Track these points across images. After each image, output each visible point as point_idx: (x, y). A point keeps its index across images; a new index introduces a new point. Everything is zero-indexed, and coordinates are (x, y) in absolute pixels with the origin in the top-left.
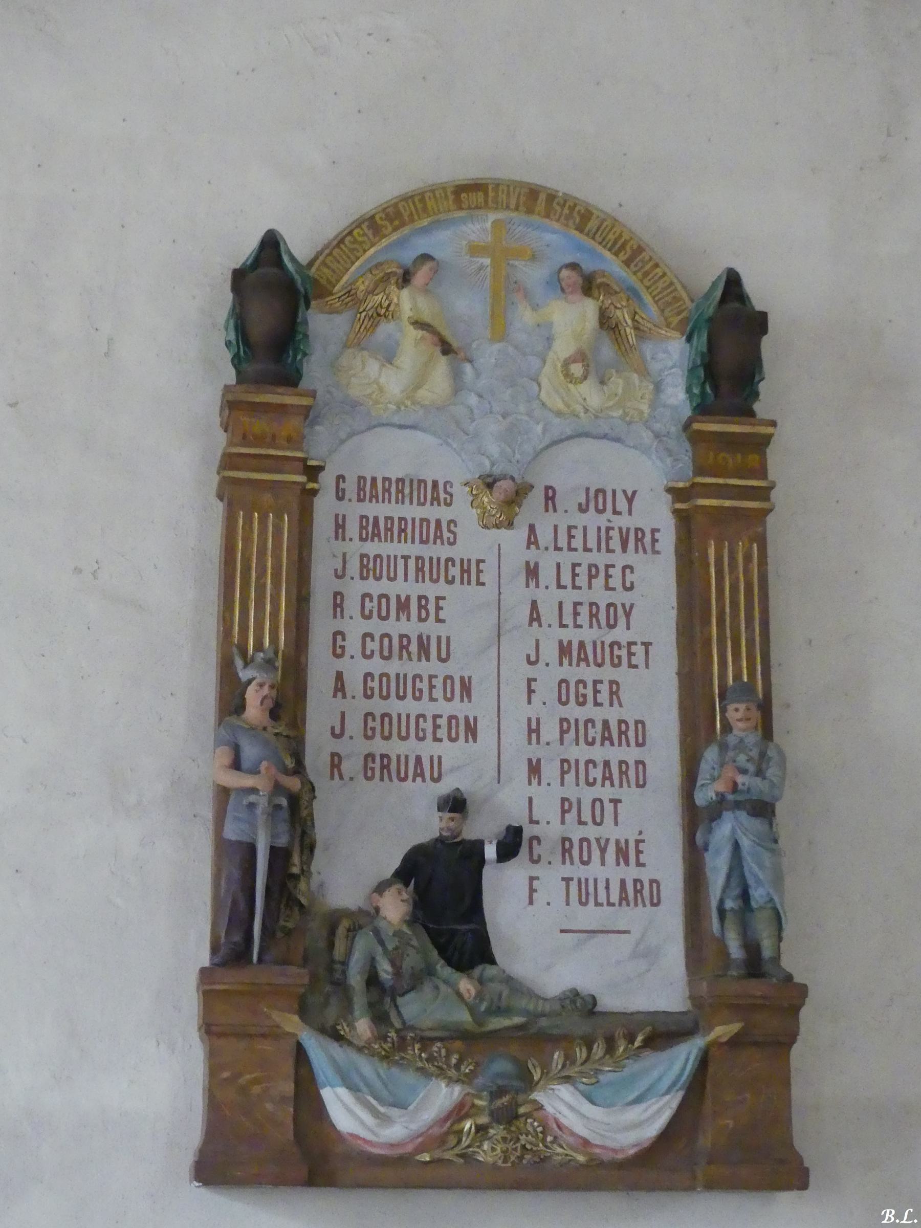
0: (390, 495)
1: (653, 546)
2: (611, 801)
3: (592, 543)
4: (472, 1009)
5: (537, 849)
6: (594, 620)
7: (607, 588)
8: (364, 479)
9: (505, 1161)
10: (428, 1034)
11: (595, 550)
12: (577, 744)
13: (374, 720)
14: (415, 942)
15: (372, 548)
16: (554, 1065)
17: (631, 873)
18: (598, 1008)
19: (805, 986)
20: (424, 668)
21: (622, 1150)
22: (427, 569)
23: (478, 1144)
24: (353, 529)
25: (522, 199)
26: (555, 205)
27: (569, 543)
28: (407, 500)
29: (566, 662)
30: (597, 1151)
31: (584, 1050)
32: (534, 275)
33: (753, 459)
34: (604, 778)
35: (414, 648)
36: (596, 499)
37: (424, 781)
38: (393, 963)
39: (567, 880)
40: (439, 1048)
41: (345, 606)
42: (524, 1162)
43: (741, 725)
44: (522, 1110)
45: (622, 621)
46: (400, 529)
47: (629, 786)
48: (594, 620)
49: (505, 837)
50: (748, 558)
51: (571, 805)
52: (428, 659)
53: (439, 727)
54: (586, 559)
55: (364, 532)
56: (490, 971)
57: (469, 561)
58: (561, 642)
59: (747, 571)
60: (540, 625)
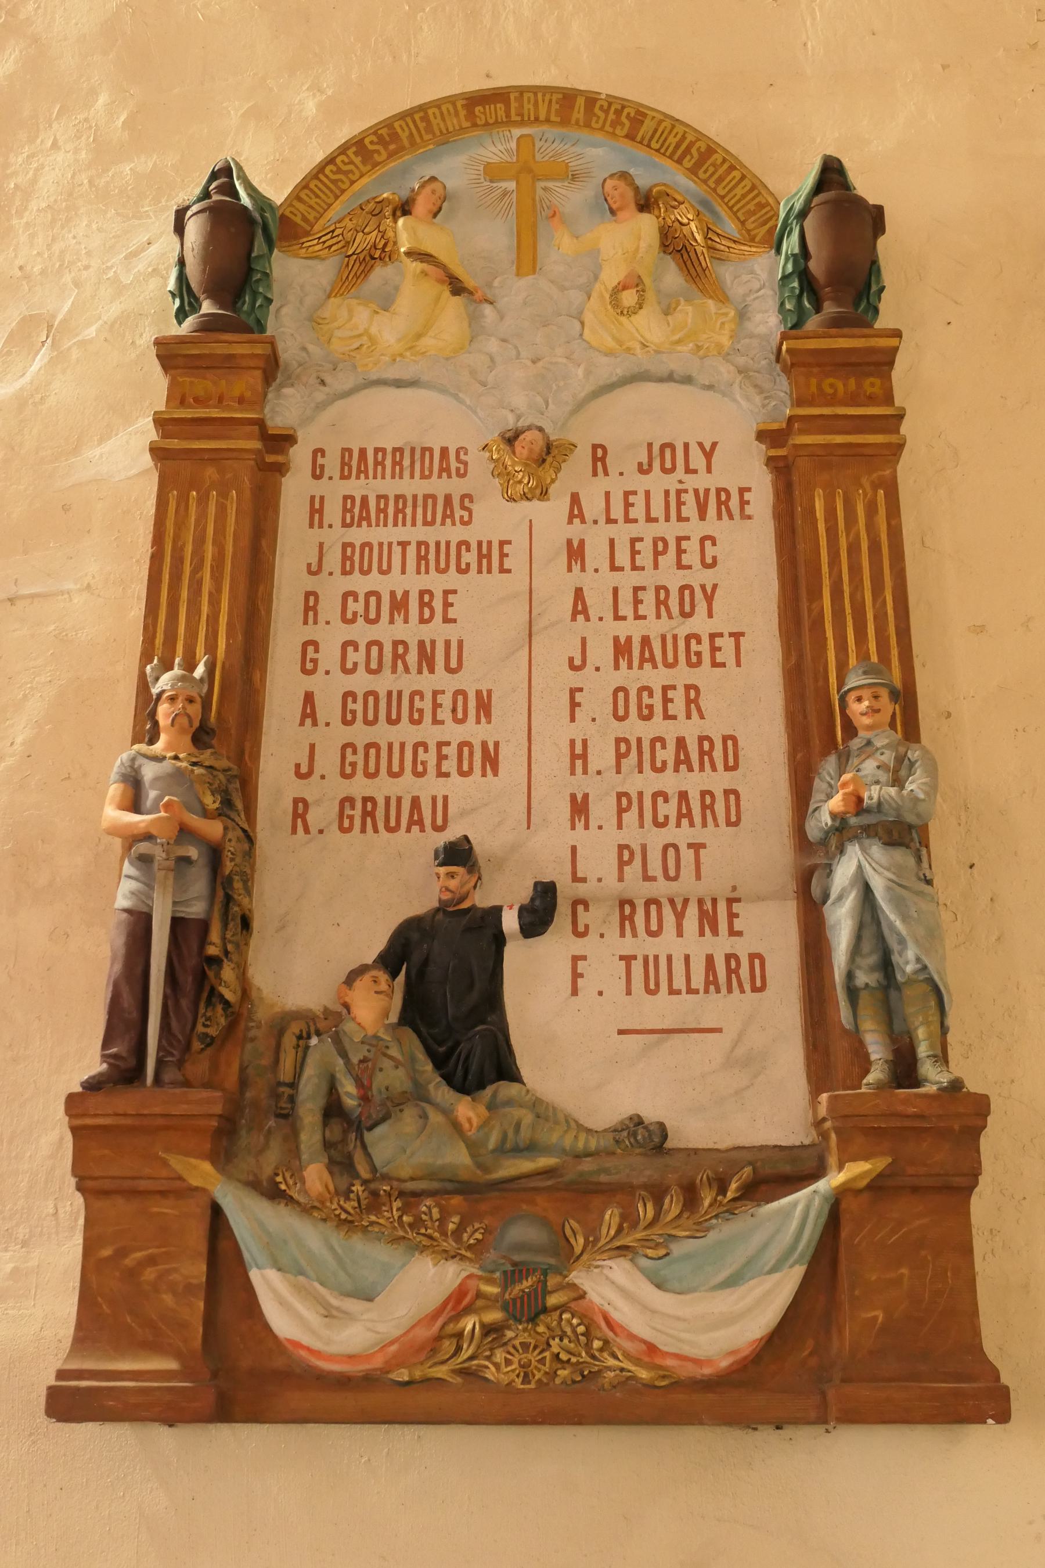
0: (384, 468)
1: (742, 509)
2: (690, 846)
3: (657, 511)
4: (473, 1147)
5: (583, 917)
6: (663, 608)
7: (680, 566)
8: (350, 451)
9: (526, 1380)
10: (410, 1186)
11: (662, 519)
12: (641, 772)
13: (355, 752)
14: (394, 1052)
15: (358, 535)
16: (604, 1230)
17: (721, 945)
18: (669, 1144)
19: (986, 1097)
20: (426, 682)
21: (709, 1362)
22: (432, 556)
23: (488, 1353)
24: (333, 512)
25: (555, 106)
26: (597, 110)
27: (626, 513)
28: (407, 473)
29: (624, 664)
30: (669, 1362)
31: (650, 1206)
32: (572, 198)
33: (872, 385)
34: (680, 816)
35: (412, 658)
36: (663, 456)
37: (422, 830)
38: (359, 1082)
39: (628, 959)
40: (429, 1208)
41: (319, 608)
42: (558, 1381)
43: (866, 721)
44: (552, 1300)
45: (702, 606)
46: (399, 509)
47: (717, 825)
48: (663, 608)
49: (532, 900)
50: (871, 509)
51: (632, 854)
52: (432, 671)
53: (446, 757)
54: (649, 532)
55: (348, 515)
56: (507, 1090)
57: (490, 543)
58: (616, 639)
59: (871, 526)
60: (587, 619)
